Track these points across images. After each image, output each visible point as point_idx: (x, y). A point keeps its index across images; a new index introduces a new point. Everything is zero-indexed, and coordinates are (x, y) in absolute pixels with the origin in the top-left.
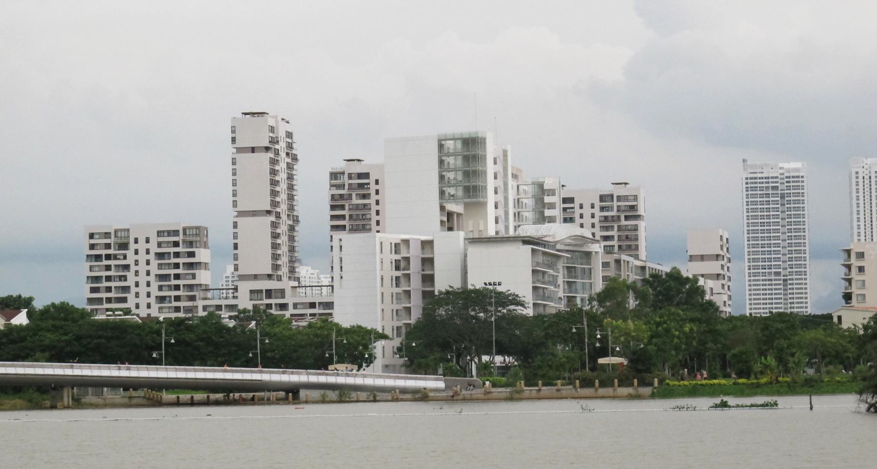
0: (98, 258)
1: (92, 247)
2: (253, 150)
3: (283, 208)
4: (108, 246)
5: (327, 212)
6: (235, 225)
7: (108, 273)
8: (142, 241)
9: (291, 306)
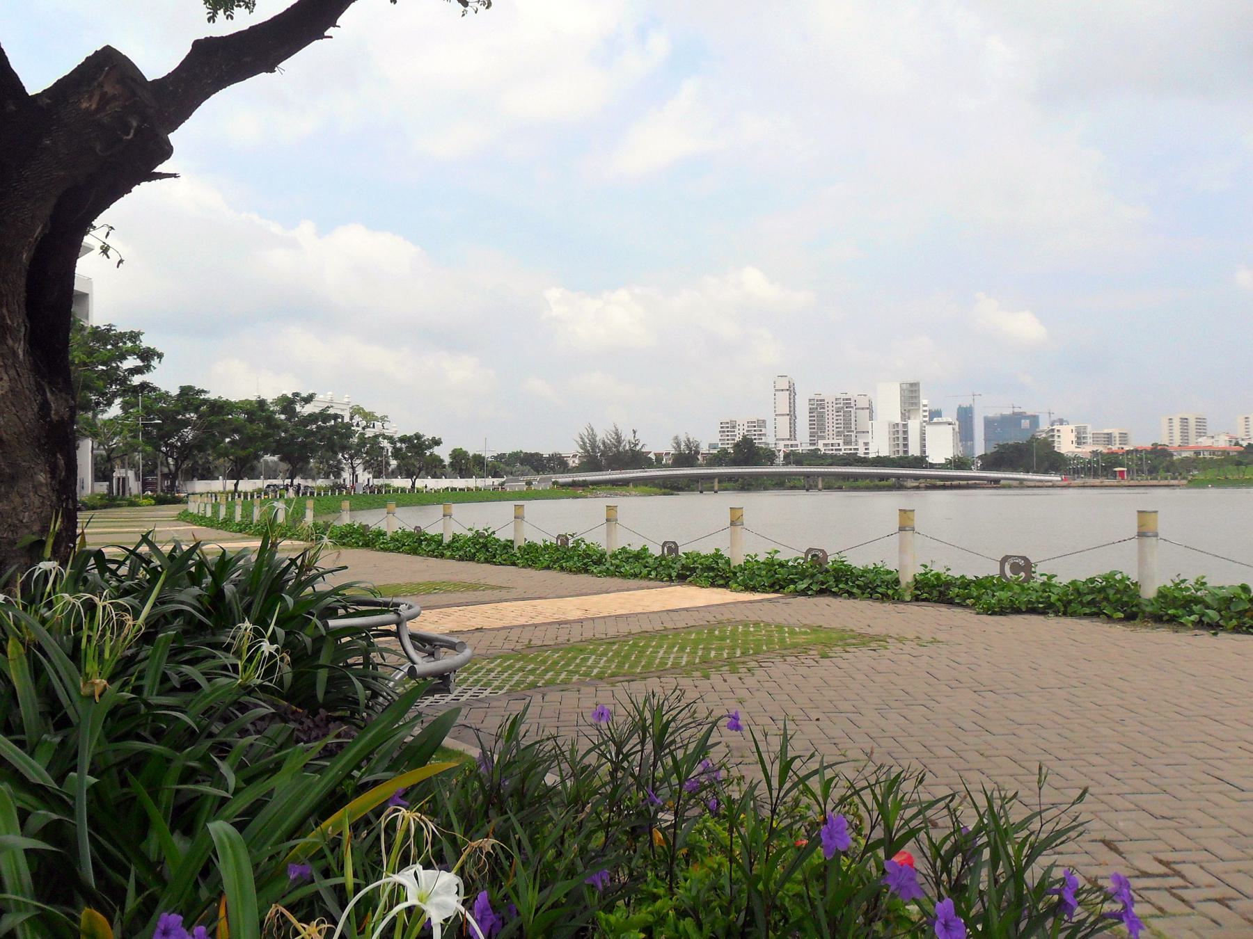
0: (724, 432)
1: (722, 427)
2: (782, 390)
3: (792, 413)
4: (728, 427)
5: (808, 414)
6: (775, 419)
8: (741, 425)
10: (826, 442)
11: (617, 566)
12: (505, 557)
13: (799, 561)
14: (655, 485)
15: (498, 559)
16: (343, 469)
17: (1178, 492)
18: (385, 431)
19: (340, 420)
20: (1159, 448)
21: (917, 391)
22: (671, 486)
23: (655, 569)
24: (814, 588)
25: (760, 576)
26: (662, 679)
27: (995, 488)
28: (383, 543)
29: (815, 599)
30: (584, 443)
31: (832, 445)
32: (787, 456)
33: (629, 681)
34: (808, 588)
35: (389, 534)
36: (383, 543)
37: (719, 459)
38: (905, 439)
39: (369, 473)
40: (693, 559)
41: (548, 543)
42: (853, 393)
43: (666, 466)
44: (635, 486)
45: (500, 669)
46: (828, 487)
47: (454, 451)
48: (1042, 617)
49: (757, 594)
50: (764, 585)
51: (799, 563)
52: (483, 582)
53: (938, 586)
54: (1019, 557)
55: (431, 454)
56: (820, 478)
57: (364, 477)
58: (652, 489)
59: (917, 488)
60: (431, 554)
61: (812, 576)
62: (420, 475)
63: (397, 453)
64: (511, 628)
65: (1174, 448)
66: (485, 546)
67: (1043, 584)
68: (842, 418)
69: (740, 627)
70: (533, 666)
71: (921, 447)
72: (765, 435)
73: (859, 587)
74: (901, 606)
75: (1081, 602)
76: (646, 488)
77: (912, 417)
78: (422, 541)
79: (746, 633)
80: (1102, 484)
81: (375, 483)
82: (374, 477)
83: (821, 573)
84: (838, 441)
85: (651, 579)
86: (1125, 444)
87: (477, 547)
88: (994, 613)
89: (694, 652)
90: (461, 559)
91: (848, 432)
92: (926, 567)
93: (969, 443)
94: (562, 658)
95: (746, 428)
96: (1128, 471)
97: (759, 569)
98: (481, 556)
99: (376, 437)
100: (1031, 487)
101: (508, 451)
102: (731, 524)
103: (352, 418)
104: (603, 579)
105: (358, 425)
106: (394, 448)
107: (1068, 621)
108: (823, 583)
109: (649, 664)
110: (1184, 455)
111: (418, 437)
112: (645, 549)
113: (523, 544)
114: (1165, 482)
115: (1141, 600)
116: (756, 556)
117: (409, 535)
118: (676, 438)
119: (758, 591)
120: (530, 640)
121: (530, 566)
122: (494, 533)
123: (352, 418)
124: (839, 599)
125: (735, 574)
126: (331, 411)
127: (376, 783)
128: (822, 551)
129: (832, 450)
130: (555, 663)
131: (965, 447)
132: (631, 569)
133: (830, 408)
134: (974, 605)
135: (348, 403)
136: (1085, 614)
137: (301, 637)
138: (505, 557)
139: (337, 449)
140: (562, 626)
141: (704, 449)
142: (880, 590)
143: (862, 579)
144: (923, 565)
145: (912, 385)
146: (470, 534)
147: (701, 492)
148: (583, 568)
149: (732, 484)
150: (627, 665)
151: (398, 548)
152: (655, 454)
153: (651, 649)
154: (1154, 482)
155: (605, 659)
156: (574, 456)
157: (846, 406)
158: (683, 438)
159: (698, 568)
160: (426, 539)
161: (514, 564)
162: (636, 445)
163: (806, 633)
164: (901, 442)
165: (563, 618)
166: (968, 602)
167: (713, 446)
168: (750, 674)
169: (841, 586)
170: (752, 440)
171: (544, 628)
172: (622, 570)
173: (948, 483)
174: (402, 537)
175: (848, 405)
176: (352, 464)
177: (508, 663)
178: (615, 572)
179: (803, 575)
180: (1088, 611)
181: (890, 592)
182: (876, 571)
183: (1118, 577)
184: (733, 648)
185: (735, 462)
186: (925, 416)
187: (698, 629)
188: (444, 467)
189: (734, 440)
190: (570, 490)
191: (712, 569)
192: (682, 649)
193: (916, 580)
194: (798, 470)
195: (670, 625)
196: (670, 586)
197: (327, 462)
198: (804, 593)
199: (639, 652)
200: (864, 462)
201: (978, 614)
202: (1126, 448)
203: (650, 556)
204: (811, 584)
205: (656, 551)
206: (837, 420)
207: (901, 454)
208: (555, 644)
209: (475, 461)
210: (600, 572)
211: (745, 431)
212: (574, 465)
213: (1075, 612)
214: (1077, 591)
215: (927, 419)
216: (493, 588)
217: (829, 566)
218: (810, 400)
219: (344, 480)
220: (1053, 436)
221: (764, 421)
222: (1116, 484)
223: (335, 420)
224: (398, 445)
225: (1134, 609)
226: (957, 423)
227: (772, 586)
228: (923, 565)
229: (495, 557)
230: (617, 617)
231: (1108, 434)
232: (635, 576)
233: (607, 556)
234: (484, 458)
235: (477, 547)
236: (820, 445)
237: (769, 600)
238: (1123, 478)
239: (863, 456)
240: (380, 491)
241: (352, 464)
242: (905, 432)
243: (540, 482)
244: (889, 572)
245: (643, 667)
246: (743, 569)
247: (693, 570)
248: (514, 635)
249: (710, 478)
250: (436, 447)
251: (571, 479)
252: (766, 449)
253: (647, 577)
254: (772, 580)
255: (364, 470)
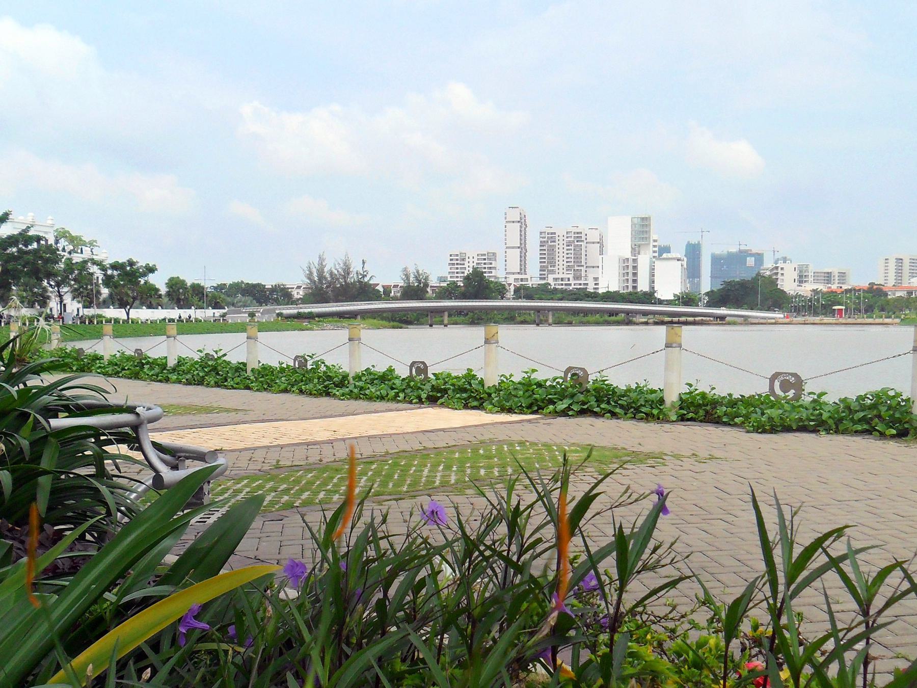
0: (453, 264)
1: (451, 260)
2: (513, 222)
4: (457, 260)
5: (539, 248)
6: (506, 252)
7: (457, 271)
8: (471, 258)
9: (573, 285)
10: (556, 276)
11: (361, 388)
12: (237, 380)
13: (557, 380)
14: (383, 319)
15: (230, 382)
16: (49, 298)
17: (891, 329)
18: (94, 257)
19: (43, 242)
20: (875, 287)
21: (648, 226)
22: (401, 319)
23: (403, 390)
24: (576, 408)
25: (516, 396)
26: (433, 497)
27: (722, 324)
28: (100, 367)
29: (576, 419)
30: (311, 273)
31: (562, 279)
32: (517, 290)
33: (396, 500)
34: (569, 408)
35: (107, 357)
36: (100, 367)
37: (449, 292)
38: (635, 274)
39: (79, 302)
40: (444, 379)
41: (284, 366)
42: (583, 227)
43: (395, 299)
44: (363, 318)
45: (248, 489)
46: (559, 322)
47: (171, 279)
48: (813, 435)
49: (514, 415)
50: (521, 406)
51: (558, 383)
52: (215, 405)
53: (705, 405)
54: (790, 374)
55: (146, 282)
56: (550, 313)
57: (73, 307)
58: (381, 322)
59: (646, 323)
60: (155, 379)
61: (572, 396)
62: (134, 304)
63: (108, 281)
64: (255, 449)
65: (889, 288)
66: (215, 369)
67: (814, 401)
68: (572, 252)
69: (505, 446)
70: (285, 486)
71: (650, 283)
72: (495, 268)
73: (622, 407)
74: (667, 426)
75: (852, 420)
76: (375, 321)
77: (642, 252)
78: (143, 364)
79: (512, 453)
80: (822, 322)
81: (86, 313)
82: (84, 307)
83: (582, 393)
84: (568, 276)
85: (399, 401)
86: (843, 283)
87: (206, 370)
88: (764, 431)
89: (461, 470)
90: (189, 383)
91: (579, 266)
92: (691, 385)
93: (696, 280)
94: (316, 478)
95: (476, 261)
96: (846, 310)
97: (515, 389)
98: (211, 379)
99: (85, 262)
100: (755, 324)
101: (228, 281)
102: (485, 343)
103: (57, 242)
104: (346, 402)
105: (64, 250)
106: (105, 275)
107: (840, 439)
108: (584, 403)
109: (415, 483)
110: (898, 294)
111: (131, 263)
112: (391, 370)
113: (256, 366)
114: (880, 321)
115: (912, 416)
116: (511, 375)
117: (129, 358)
118: (405, 269)
119: (516, 413)
120: (278, 461)
121: (265, 390)
122: (225, 355)
123: (57, 242)
124: (601, 420)
125: (489, 395)
126: (31, 233)
127: (146, 602)
128: (583, 369)
129: (562, 285)
130: (310, 483)
131: (692, 283)
132: (376, 391)
133: (561, 242)
134: (743, 423)
135: (52, 226)
136: (856, 432)
137: (16, 439)
138: (237, 380)
139: (41, 275)
140: (310, 447)
141: (433, 282)
142: (643, 409)
143: (625, 399)
144: (687, 384)
145: (643, 219)
146: (197, 358)
147: (431, 326)
148: (324, 391)
149: (462, 318)
150: (391, 485)
151: (118, 373)
152: (383, 287)
153: (414, 468)
154: (870, 320)
155: (365, 478)
156: (299, 287)
157: (577, 240)
158: (412, 270)
159: (449, 389)
160: (148, 363)
161: (248, 388)
162: (364, 276)
163: (577, 451)
164: (630, 277)
165: (310, 439)
166: (737, 420)
167: (442, 279)
168: (528, 491)
169: (603, 406)
170: (483, 273)
171: (292, 449)
172: (367, 392)
173: (676, 319)
174: (121, 361)
175: (579, 239)
176: (59, 292)
177: (257, 483)
178: (360, 395)
179: (562, 395)
180: (859, 428)
181: (655, 412)
182: (639, 390)
183: (892, 393)
184: (503, 467)
185: (464, 296)
186: (654, 252)
187: (462, 449)
188: (160, 296)
189: (463, 273)
190: (295, 323)
191: (464, 390)
192: (448, 467)
193: (681, 399)
194: (529, 304)
195: (430, 445)
196: (419, 408)
197: (31, 291)
198: (564, 413)
199: (402, 471)
200: (594, 297)
201: (748, 432)
202: (845, 287)
203: (396, 378)
204: (571, 404)
205: (403, 372)
206: (567, 254)
207: (630, 289)
208: (306, 465)
209: (193, 290)
210: (343, 395)
211: (475, 264)
212: (299, 297)
213: (846, 429)
214: (848, 408)
215: (656, 254)
216: (227, 410)
217: (589, 386)
218: (541, 233)
219: (51, 310)
220: (777, 274)
221: (494, 254)
222: (834, 321)
223: (38, 242)
224: (109, 272)
225: (906, 426)
226: (685, 259)
227: (530, 406)
228: (687, 384)
229: (226, 380)
230: (369, 437)
231: (828, 273)
232: (382, 398)
233: (350, 378)
234: (203, 288)
235: (206, 370)
236: (550, 280)
237: (529, 421)
238: (841, 317)
239: (592, 291)
240: (91, 322)
241: (59, 292)
242: (635, 268)
243: (264, 313)
244: (653, 392)
245: (409, 485)
246: (498, 390)
247: (445, 391)
248: (259, 456)
249: (439, 311)
250: (151, 275)
251: (295, 311)
252: (496, 282)
253: (395, 399)
254: (530, 401)
255: (74, 298)
